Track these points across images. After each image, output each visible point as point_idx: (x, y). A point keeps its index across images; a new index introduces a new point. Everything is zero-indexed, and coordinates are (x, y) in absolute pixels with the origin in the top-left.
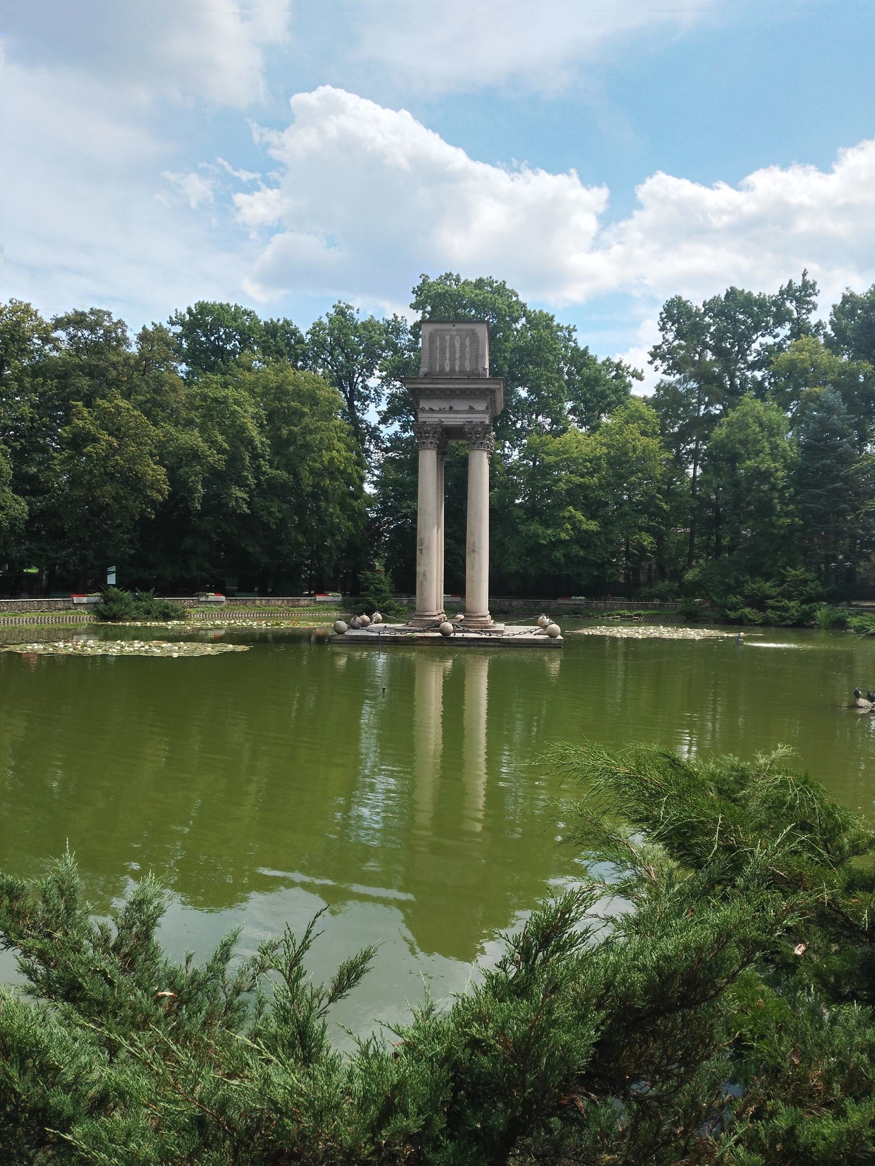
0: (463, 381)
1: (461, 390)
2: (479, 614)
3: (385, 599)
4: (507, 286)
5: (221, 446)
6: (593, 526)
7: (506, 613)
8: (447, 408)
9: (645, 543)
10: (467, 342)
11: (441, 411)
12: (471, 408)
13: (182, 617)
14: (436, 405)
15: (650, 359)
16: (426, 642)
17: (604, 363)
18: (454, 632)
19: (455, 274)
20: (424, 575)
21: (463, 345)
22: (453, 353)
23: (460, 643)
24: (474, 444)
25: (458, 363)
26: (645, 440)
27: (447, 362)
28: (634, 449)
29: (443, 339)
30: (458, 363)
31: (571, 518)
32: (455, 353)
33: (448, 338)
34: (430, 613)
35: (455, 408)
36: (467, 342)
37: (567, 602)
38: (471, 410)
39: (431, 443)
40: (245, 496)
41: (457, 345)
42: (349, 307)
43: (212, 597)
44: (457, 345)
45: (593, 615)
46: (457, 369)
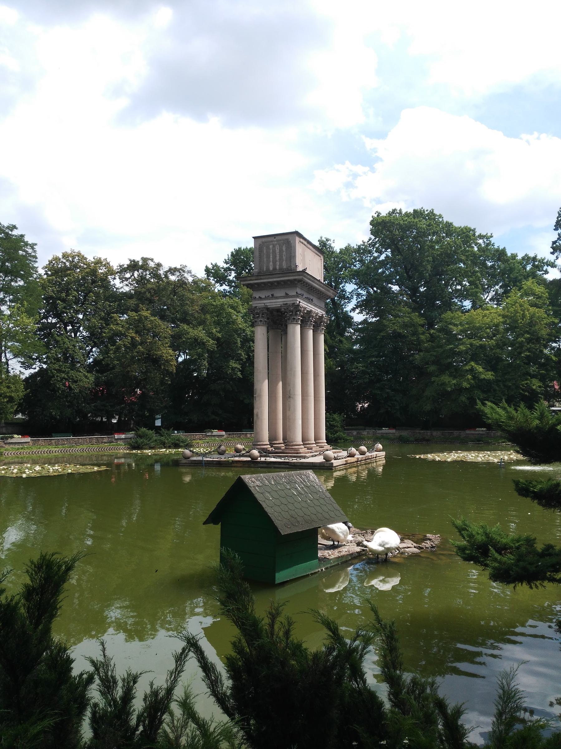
0: (275, 276)
1: (278, 282)
2: (294, 443)
3: (337, 432)
4: (435, 212)
5: (216, 335)
6: (489, 375)
7: (428, 440)
8: (283, 294)
9: (534, 387)
10: (284, 249)
11: (267, 298)
12: (287, 294)
13: (188, 446)
14: (263, 294)
15: (552, 251)
16: (239, 465)
17: (523, 258)
18: (261, 456)
19: (398, 209)
20: (257, 415)
21: (281, 251)
22: (275, 257)
23: (262, 465)
24: (289, 319)
25: (278, 263)
26: (532, 309)
27: (271, 263)
28: (524, 316)
29: (268, 248)
30: (278, 263)
31: (472, 370)
32: (276, 257)
33: (271, 246)
34: (261, 443)
35: (275, 295)
36: (284, 249)
37: (473, 432)
38: (287, 296)
39: (261, 321)
40: (239, 366)
41: (277, 251)
42: (327, 240)
43: (216, 432)
44: (277, 251)
45: (491, 442)
46: (278, 267)
